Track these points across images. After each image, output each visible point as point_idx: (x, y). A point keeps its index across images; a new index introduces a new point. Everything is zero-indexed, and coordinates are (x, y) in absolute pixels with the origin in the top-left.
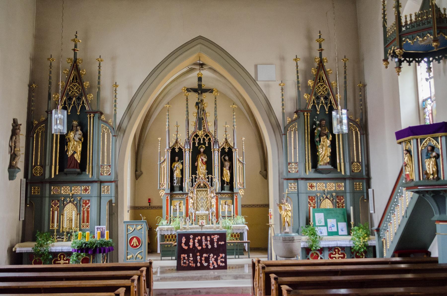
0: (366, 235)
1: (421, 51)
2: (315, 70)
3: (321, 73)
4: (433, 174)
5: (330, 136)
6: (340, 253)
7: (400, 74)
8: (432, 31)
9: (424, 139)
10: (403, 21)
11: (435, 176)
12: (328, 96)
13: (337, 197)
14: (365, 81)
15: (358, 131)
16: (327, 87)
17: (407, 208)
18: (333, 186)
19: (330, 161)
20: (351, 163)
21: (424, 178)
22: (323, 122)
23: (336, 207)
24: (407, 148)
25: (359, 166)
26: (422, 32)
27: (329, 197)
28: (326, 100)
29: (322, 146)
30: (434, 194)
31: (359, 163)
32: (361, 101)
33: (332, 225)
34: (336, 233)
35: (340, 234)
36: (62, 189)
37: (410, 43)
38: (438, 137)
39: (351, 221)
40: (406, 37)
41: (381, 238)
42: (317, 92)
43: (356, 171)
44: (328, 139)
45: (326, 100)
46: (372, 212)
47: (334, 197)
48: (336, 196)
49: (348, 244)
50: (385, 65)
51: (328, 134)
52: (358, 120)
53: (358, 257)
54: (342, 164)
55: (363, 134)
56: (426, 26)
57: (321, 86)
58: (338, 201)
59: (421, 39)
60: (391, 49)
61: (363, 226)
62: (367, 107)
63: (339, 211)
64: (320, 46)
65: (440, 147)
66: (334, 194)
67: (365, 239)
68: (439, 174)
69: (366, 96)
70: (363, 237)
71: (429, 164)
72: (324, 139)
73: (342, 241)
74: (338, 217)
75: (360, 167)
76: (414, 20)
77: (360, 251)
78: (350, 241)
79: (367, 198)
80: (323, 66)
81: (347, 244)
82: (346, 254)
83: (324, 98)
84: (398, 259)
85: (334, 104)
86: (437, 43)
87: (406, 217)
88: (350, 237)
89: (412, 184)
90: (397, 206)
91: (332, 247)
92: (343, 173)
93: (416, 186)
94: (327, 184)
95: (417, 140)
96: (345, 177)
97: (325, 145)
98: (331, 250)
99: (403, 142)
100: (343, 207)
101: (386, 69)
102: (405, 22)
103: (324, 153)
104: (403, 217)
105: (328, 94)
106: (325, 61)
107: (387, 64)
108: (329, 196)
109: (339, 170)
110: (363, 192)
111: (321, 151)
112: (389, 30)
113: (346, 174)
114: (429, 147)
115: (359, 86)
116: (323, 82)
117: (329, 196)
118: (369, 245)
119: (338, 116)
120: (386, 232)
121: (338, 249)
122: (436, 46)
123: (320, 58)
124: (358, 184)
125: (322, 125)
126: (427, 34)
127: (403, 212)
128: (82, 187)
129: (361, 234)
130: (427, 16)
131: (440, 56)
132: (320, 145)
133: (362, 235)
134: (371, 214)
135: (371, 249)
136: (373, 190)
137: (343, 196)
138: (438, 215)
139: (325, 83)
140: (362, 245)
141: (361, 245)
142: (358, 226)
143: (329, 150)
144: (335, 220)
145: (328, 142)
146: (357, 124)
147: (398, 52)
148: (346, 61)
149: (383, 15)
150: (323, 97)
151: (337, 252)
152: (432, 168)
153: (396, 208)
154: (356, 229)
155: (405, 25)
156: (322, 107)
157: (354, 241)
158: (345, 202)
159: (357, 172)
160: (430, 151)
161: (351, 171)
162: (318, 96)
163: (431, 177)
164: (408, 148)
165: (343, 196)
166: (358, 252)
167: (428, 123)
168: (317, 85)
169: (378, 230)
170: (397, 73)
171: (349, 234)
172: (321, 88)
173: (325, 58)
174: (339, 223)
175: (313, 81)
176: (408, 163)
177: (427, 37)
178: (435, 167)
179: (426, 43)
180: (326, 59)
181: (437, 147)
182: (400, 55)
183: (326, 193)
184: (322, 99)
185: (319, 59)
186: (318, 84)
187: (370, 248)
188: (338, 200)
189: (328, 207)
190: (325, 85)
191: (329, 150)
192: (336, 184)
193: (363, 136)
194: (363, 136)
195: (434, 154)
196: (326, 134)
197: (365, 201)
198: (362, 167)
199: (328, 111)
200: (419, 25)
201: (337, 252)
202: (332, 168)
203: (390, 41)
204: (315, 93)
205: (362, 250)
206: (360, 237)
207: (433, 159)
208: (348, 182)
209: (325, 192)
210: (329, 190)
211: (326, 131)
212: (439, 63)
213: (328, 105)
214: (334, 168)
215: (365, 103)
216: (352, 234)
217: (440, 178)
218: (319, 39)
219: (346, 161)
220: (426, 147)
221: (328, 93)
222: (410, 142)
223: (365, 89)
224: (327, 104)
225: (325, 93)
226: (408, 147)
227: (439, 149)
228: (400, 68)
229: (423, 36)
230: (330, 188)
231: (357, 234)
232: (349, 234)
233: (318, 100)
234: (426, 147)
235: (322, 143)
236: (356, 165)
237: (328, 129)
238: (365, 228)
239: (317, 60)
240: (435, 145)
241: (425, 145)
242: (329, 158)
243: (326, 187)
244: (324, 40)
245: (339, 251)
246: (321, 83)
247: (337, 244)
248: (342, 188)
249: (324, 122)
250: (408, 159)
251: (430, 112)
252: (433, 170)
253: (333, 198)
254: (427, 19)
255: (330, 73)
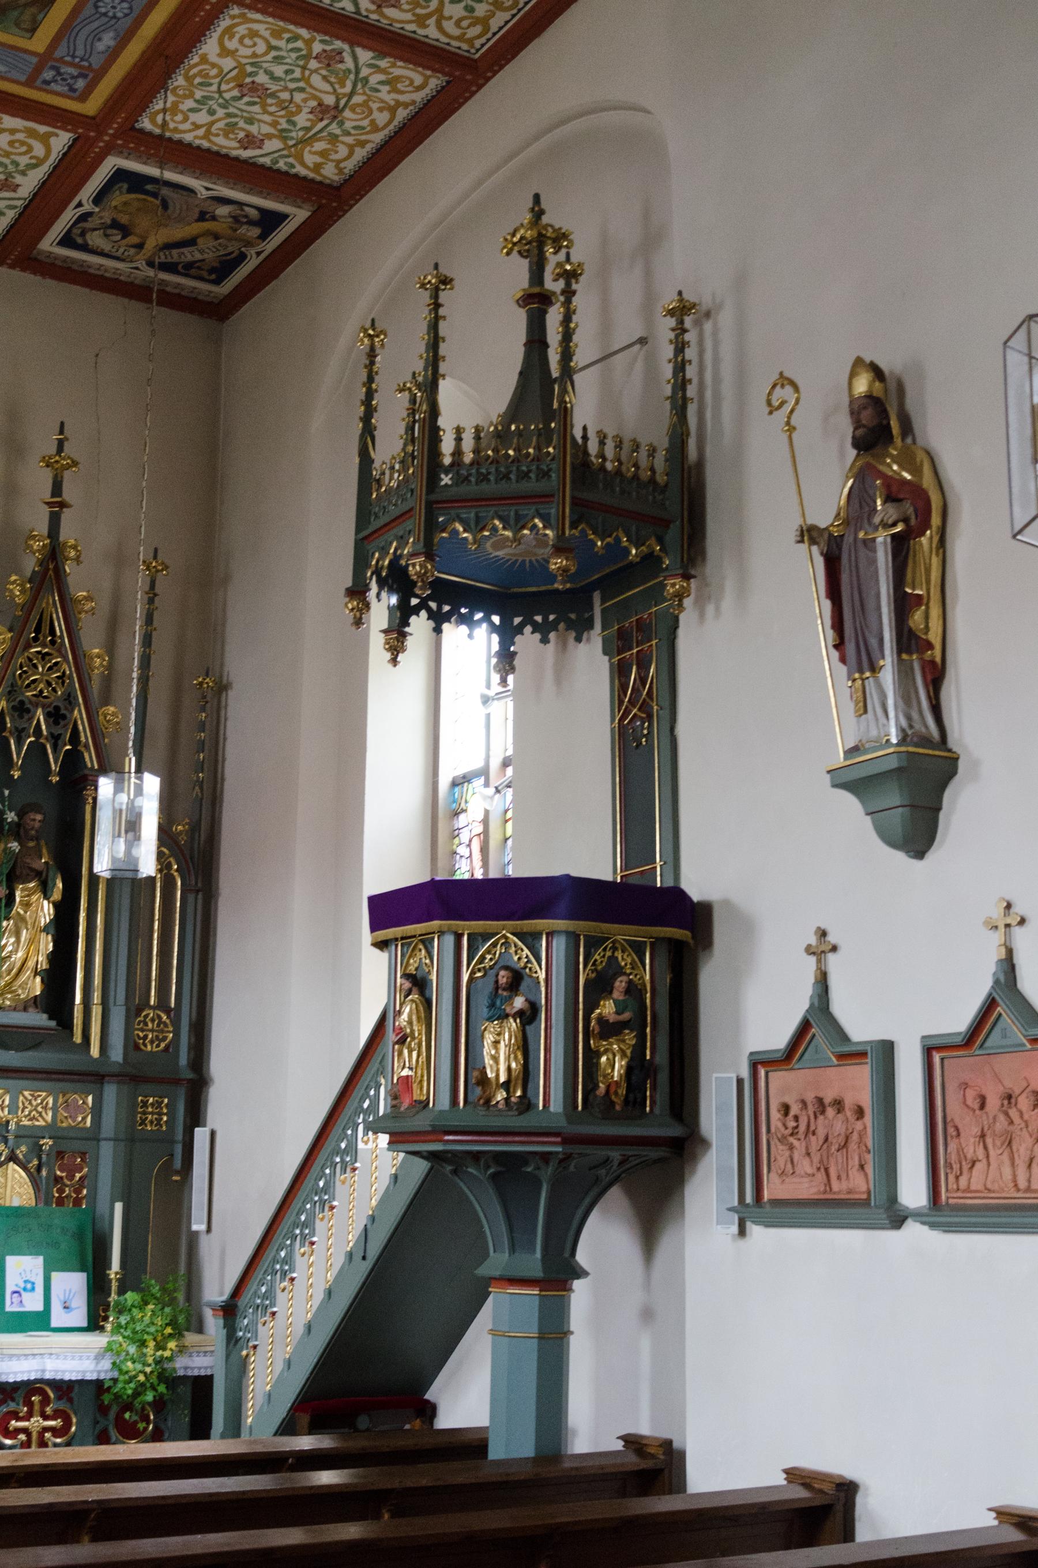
0: (169, 1330)
1: (487, 584)
2: (22, 585)
3: (48, 603)
4: (506, 1086)
5: (55, 884)
6: (49, 1410)
7: (399, 659)
8: (553, 511)
9: (486, 936)
10: (447, 446)
11: (515, 1092)
12: (66, 709)
13: (60, 1154)
14: (226, 669)
15: (176, 874)
16: (65, 666)
17: (373, 1218)
18: (45, 1108)
19: (42, 992)
20: (135, 1009)
21: (470, 1098)
22: (32, 816)
23: (47, 1203)
24: (411, 969)
25: (165, 1023)
26: (514, 508)
27: (21, 1156)
28: (56, 723)
29: (16, 925)
30: (499, 1169)
31: (168, 1011)
32: (201, 746)
33: (26, 1282)
34: (39, 1322)
35: (54, 1324)
36: (50, 1114)
37: (466, 539)
38: (536, 936)
39: (110, 1269)
40: (453, 512)
41: (238, 1346)
42: (19, 683)
43: (149, 1048)
44: (46, 897)
45: (56, 723)
46: (198, 1226)
47: (44, 1157)
48: (54, 1153)
49: (92, 1372)
50: (352, 610)
51: (51, 874)
52: (180, 828)
53: (130, 1433)
54: (96, 1012)
55: (198, 891)
56: (531, 485)
57: (43, 659)
58: (58, 1173)
59: (508, 533)
60: (384, 551)
61: (163, 1289)
62: (223, 779)
63: (62, 1218)
64: (57, 488)
65: (542, 975)
66: (47, 1143)
67: (164, 1349)
68: (530, 1085)
69: (222, 727)
70: (159, 1338)
71: (496, 1043)
72: (28, 896)
73: (65, 1358)
74: (56, 1245)
75: (171, 1029)
76: (472, 455)
77: (139, 1399)
78: (99, 1357)
79: (183, 1164)
80: (59, 576)
81: (84, 1372)
82: (76, 1414)
83: (48, 715)
84: (305, 1443)
85: (87, 746)
86: (567, 559)
87: (364, 1258)
88: (98, 1341)
89: (421, 1122)
90: (327, 1208)
91: (15, 1382)
92: (95, 1051)
93: (438, 1131)
94: (21, 1098)
95: (458, 937)
96: (103, 1070)
97: (30, 921)
98: (13, 1400)
99: (396, 939)
100: (77, 1202)
101: (354, 628)
102: (453, 454)
103: (20, 954)
104: (350, 1255)
105: (69, 699)
106: (73, 553)
107: (360, 610)
108: (24, 1148)
109: (78, 1038)
110: (168, 1140)
111: (9, 948)
112: (383, 473)
113: (108, 1057)
114: (502, 973)
115: (201, 684)
116: (53, 642)
117: (21, 1151)
118: (181, 1373)
119: (123, 798)
120: (268, 1318)
121: (42, 1392)
122: (565, 570)
123: (49, 536)
124: (152, 1105)
125: (26, 831)
126: (533, 518)
127: (353, 1237)
128: (61, 1096)
129: (153, 1324)
130: (538, 448)
131: (552, 617)
132: (8, 919)
133: (152, 1329)
134: (194, 1237)
135: (185, 1391)
136: (213, 1134)
137: (84, 1154)
138: (507, 1255)
139: (59, 651)
140: (152, 1372)
141: (145, 1374)
142: (136, 1289)
143: (47, 944)
144: (40, 1259)
145: (46, 911)
146: (177, 843)
147: (418, 568)
148: (158, 571)
149: (363, 408)
150: (43, 707)
151: (37, 1407)
152: (508, 1059)
153: (322, 1219)
154: (129, 1303)
155: (452, 465)
156: (37, 751)
157: (118, 1354)
158: (90, 1181)
159: (155, 1050)
160: (504, 989)
161: (132, 1045)
162: (22, 703)
163: (500, 1096)
164: (417, 969)
165: (83, 1154)
166: (128, 1407)
167: (463, 873)
168: (26, 654)
169: (229, 1311)
170: (388, 656)
171: (95, 1324)
172: (40, 669)
173: (72, 542)
174: (55, 1276)
175: (10, 630)
176: (412, 1031)
177: (531, 530)
178: (520, 1056)
179: (515, 555)
180: (74, 547)
181: (531, 977)
182: (423, 581)
183: (11, 1137)
184: (40, 714)
185: (47, 541)
186: (28, 646)
187: (181, 1389)
188: (62, 1171)
189: (16, 1202)
190: (59, 660)
191: (47, 944)
192: (60, 1100)
193: (196, 899)
194: (196, 899)
195: (519, 1002)
196: (38, 874)
197: (176, 1178)
198: (177, 1034)
199: (59, 774)
200: (506, 477)
201: (37, 1407)
202: (53, 1024)
203: (384, 520)
204: (12, 685)
205: (149, 1397)
206: (146, 1337)
207: (513, 1024)
208: (111, 1092)
209: (8, 1131)
210: (26, 1122)
211: (43, 861)
212: (545, 640)
213: (65, 745)
214: (58, 1024)
215: (216, 761)
216: (109, 1327)
217: (533, 1101)
218: (57, 458)
219: (111, 1000)
220: (493, 972)
221: (69, 695)
222: (427, 943)
223: (223, 704)
224: (60, 742)
225: (54, 690)
226: (416, 965)
227: (539, 983)
228: (402, 636)
229: (518, 524)
230: (34, 1113)
231: (131, 1326)
232: (95, 1324)
233: (21, 717)
234: (493, 972)
235: (18, 909)
236: (153, 1020)
237: (49, 853)
238: (167, 1300)
239: (37, 545)
240: (525, 967)
241: (487, 963)
242: (42, 981)
243: (13, 1108)
244: (75, 463)
245: (46, 1401)
246: (44, 646)
247: (43, 1371)
248: (84, 1119)
249: (39, 817)
250: (414, 1017)
251: (480, 829)
252: (509, 1069)
253: (40, 1159)
254: (537, 459)
255: (86, 612)
